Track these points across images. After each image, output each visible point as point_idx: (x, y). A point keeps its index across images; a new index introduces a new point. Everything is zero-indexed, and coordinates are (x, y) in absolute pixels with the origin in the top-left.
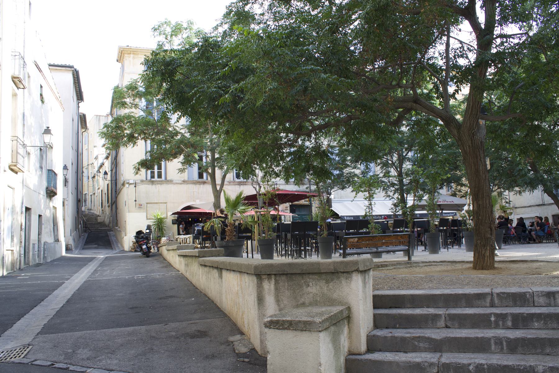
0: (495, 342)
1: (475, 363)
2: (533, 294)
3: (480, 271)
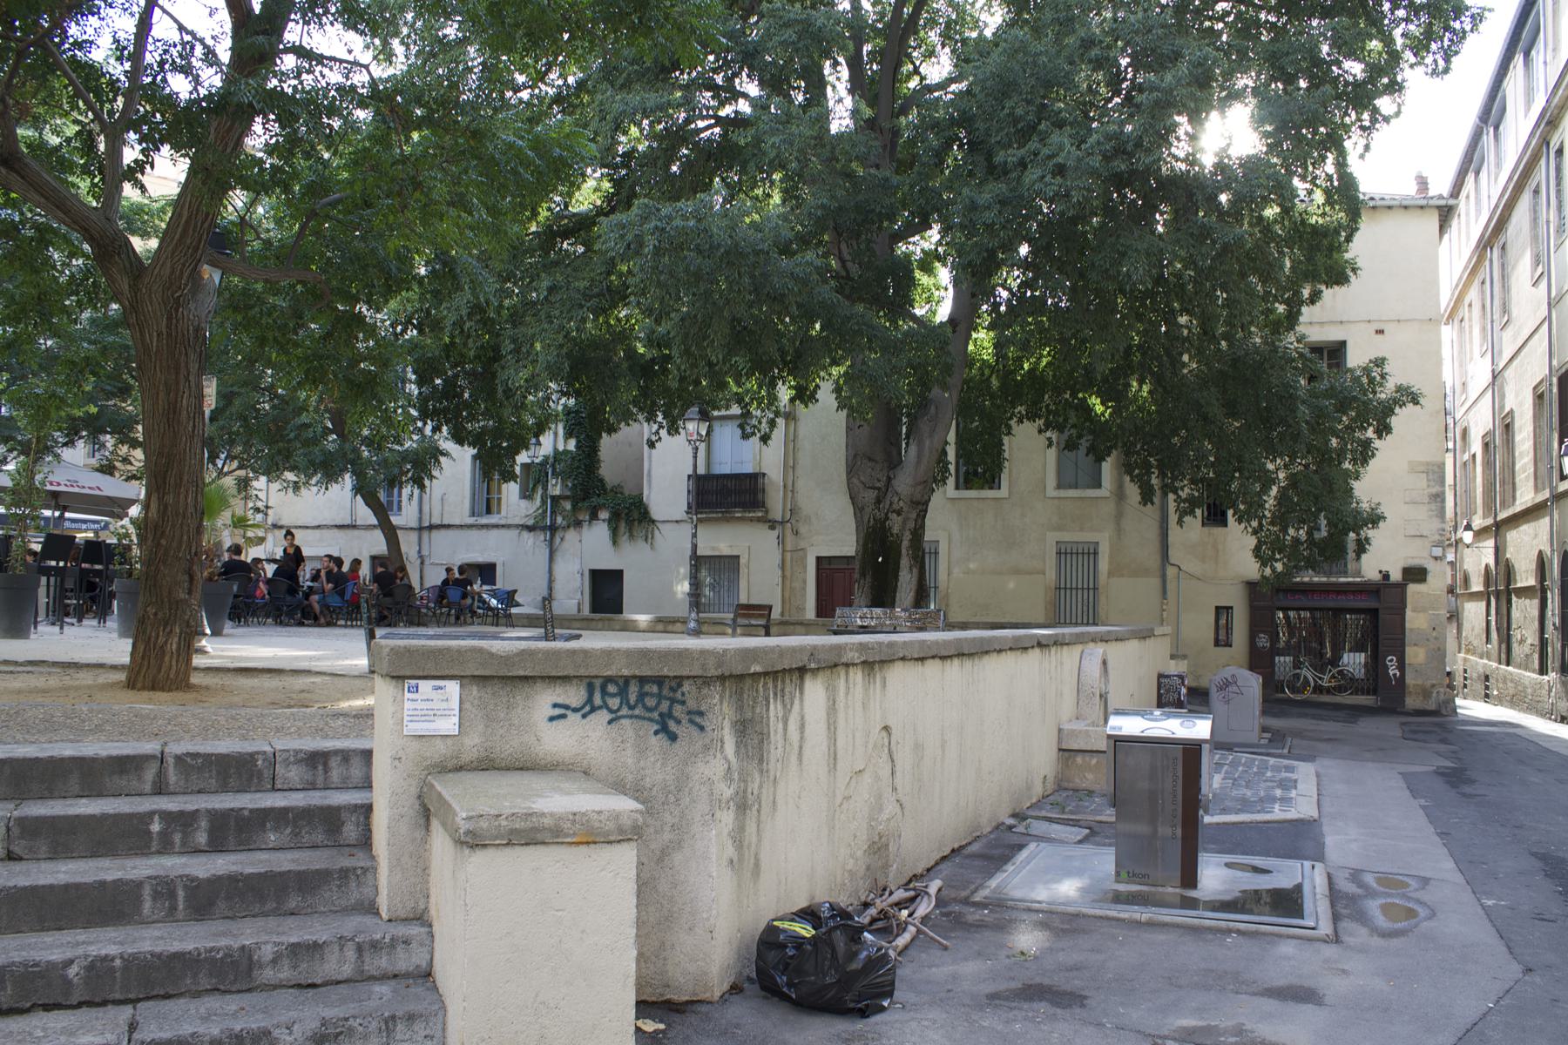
0: (155, 891)
1: (86, 956)
2: (272, 759)
3: (146, 694)
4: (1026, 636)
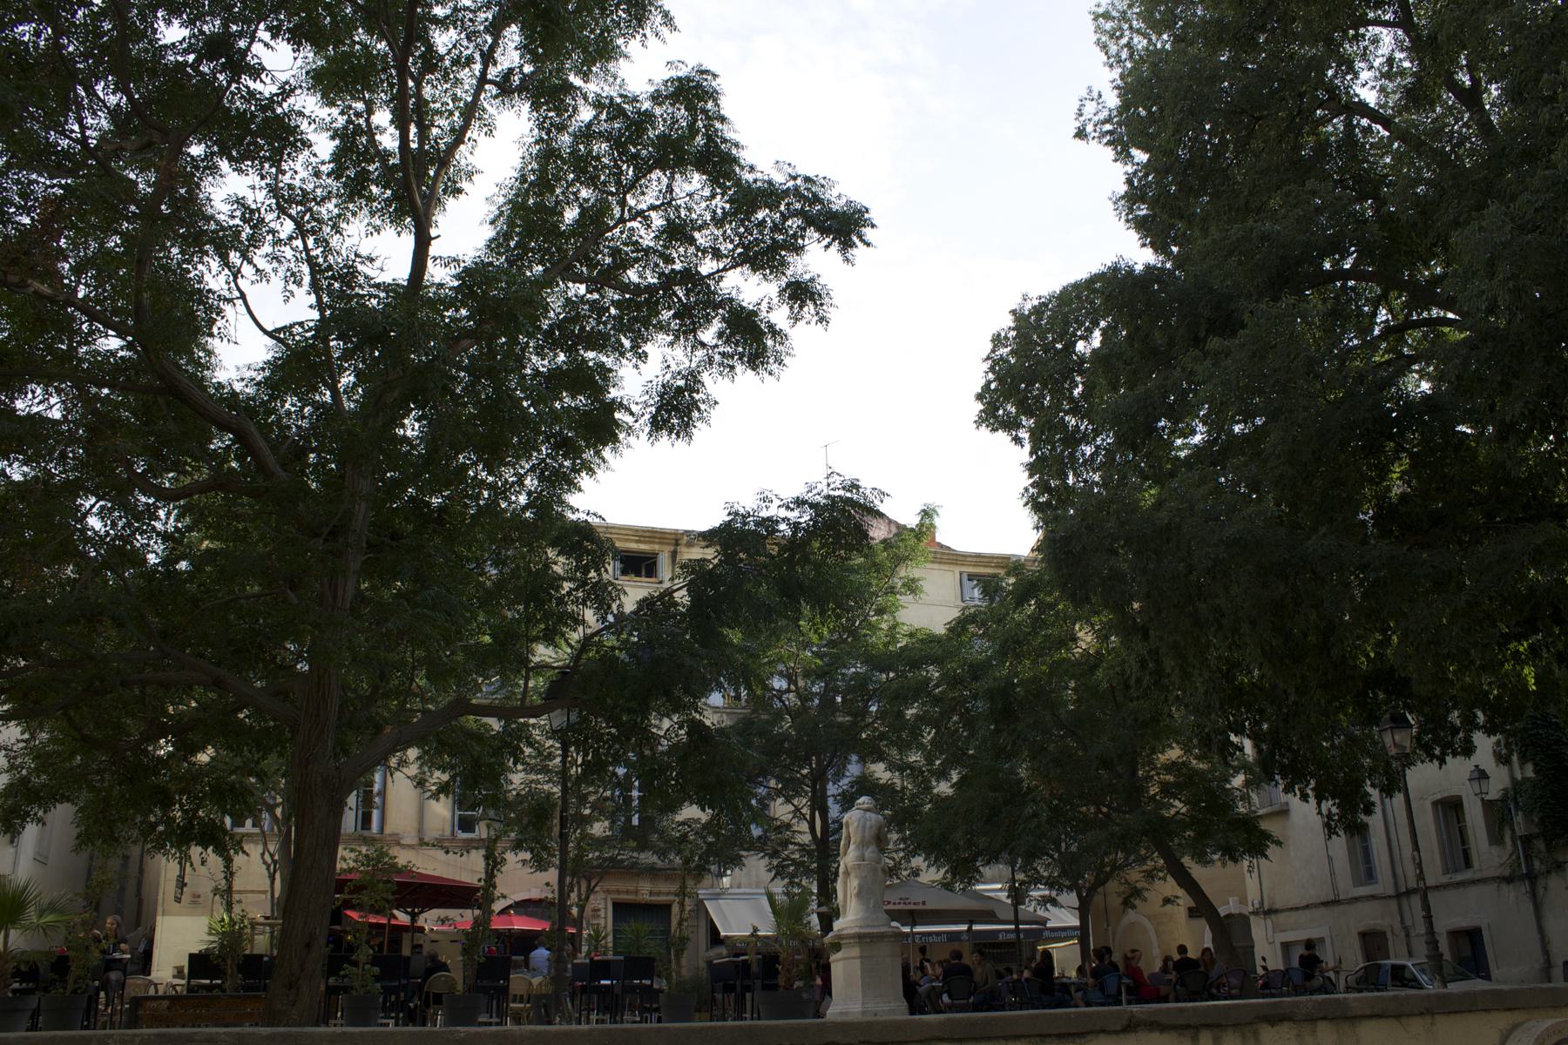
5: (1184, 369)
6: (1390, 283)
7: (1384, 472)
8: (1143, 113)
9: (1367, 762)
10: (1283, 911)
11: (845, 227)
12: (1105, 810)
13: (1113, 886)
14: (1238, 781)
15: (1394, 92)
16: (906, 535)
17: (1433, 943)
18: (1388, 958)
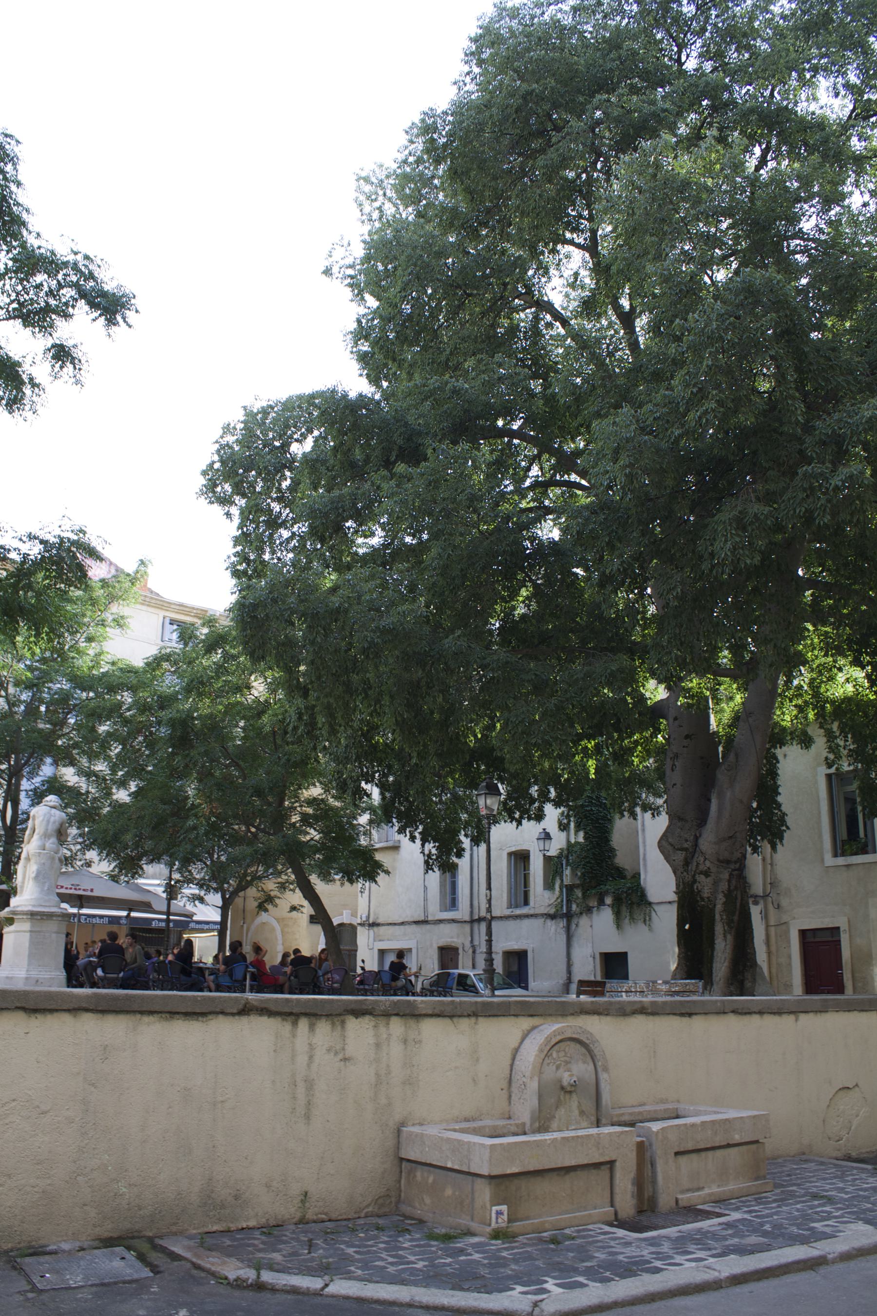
4: (338, 1000)
5: (373, 484)
6: (545, 447)
7: (514, 594)
8: (380, 267)
9: (464, 816)
10: (383, 925)
11: (111, 306)
12: (253, 830)
13: (252, 892)
14: (364, 819)
15: (574, 300)
16: (122, 578)
17: (490, 961)
18: (457, 968)
